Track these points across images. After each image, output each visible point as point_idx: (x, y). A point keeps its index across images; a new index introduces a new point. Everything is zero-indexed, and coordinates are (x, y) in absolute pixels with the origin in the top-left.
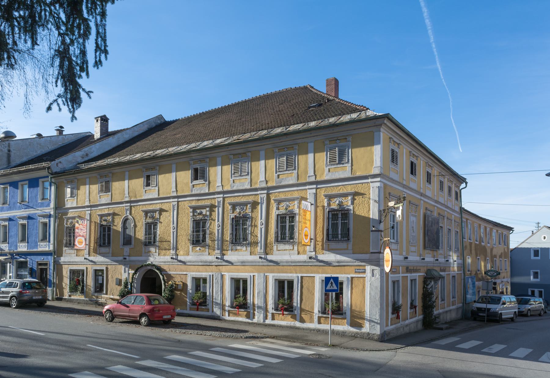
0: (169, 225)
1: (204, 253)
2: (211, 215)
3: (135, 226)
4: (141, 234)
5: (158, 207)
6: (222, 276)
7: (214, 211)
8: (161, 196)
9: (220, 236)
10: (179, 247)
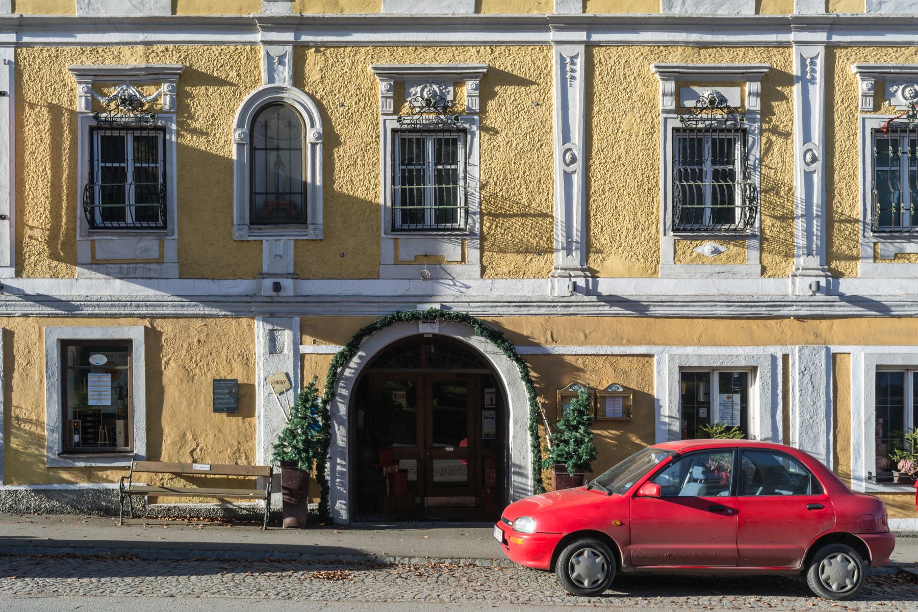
0: (539, 144)
1: (738, 268)
2: (767, 112)
3: (330, 139)
4: (369, 177)
5: (475, 60)
6: (833, 360)
7: (782, 97)
9: (817, 199)
10: (601, 238)
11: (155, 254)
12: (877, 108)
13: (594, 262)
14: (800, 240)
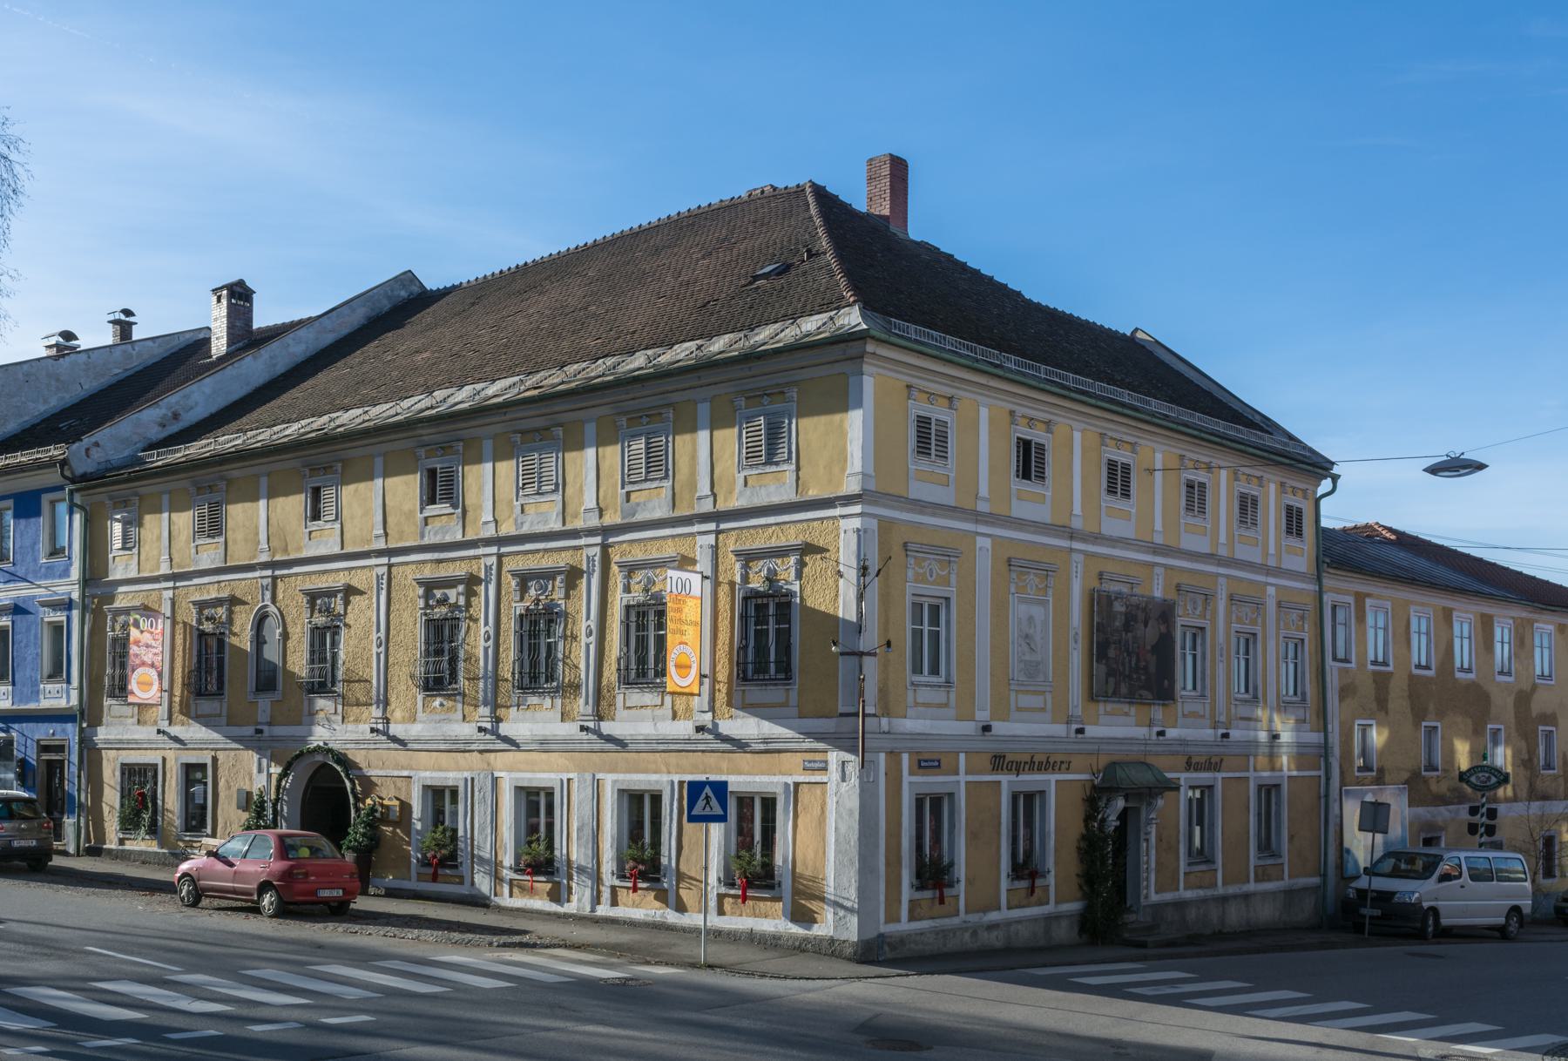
2: (468, 605)
8: (349, 549)
9: (490, 668)
10: (393, 699)
11: (944, 700)
12: (522, 599)
13: (501, 712)
14: (481, 696)
